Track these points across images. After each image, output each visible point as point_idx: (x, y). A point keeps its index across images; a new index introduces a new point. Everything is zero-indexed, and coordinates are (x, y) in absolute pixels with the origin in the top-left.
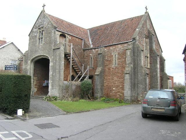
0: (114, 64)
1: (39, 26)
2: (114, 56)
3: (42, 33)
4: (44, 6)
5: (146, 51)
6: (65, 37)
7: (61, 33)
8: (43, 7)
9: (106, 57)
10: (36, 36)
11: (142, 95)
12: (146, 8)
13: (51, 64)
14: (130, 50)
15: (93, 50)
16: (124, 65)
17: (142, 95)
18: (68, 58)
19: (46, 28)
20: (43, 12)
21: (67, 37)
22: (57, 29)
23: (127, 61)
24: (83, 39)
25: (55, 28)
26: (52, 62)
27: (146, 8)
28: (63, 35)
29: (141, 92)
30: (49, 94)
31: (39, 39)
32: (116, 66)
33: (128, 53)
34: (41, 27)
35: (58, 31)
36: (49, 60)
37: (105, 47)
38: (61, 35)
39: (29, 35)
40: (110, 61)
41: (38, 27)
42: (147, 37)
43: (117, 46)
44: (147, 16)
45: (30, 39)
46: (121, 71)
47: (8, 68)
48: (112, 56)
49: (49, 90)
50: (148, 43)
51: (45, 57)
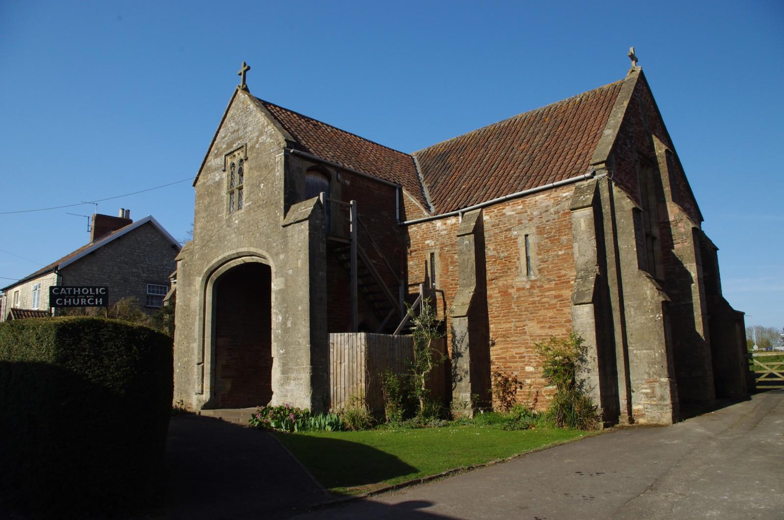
0: (525, 272)
1: (229, 145)
2: (521, 240)
3: (241, 172)
7: (313, 164)
10: (219, 184)
17: (648, 391)
18: (344, 257)
19: (253, 147)
23: (577, 255)
29: (646, 377)
32: (533, 278)
34: (235, 146)
36: (267, 269)
41: (227, 149)
43: (530, 200)
46: (556, 297)
47: (63, 296)
48: (514, 240)
49: (275, 386)
51: (255, 259)
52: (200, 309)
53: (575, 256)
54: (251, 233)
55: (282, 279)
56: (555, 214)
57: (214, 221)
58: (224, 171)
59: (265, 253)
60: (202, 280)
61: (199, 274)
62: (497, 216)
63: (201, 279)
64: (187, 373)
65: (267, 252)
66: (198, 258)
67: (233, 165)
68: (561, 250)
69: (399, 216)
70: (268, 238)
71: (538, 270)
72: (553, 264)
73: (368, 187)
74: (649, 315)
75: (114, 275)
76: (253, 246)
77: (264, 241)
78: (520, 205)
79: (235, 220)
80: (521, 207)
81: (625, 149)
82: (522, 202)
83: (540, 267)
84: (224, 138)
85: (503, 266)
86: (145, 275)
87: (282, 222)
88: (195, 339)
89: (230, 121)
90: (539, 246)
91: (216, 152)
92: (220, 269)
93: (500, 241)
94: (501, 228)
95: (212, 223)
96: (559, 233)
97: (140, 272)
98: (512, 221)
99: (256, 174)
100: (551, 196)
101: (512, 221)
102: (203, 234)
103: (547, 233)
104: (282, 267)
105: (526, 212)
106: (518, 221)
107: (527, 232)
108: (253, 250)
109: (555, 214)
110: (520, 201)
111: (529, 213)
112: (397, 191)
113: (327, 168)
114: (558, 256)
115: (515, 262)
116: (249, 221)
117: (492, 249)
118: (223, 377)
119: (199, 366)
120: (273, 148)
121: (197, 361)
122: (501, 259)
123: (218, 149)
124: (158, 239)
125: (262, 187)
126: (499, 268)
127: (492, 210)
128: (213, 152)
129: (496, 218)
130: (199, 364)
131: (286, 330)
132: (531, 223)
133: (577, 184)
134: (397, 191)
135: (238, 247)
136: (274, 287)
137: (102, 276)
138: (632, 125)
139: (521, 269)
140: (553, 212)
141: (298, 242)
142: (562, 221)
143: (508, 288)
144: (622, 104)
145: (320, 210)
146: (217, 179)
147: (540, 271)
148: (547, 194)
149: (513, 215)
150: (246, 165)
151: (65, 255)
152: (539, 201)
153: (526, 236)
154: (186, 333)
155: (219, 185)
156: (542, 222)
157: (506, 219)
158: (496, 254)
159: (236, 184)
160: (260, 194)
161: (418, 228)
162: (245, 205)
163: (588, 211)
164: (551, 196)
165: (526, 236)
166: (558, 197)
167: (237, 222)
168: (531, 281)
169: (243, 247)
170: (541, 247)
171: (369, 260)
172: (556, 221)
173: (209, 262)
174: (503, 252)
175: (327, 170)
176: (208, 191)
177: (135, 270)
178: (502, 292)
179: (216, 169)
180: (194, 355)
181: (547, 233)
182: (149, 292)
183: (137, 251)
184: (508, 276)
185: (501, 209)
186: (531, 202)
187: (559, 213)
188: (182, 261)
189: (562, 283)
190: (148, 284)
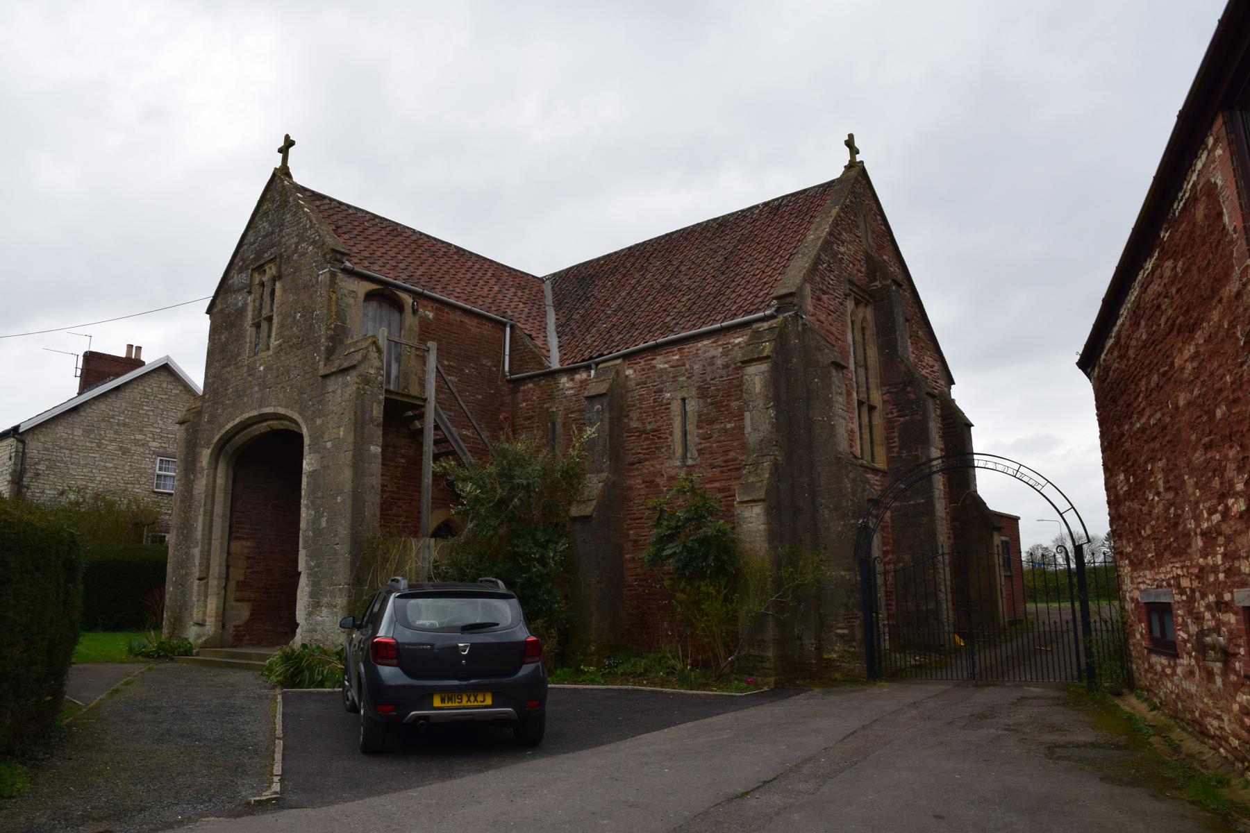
2: (676, 407)
4: (289, 143)
5: (861, 372)
6: (399, 306)
8: (280, 151)
9: (635, 415)
11: (846, 631)
12: (850, 143)
13: (308, 464)
14: (764, 367)
15: (564, 379)
16: (732, 455)
20: (282, 173)
21: (408, 309)
22: (348, 264)
23: (748, 429)
24: (504, 325)
25: (337, 256)
26: (316, 447)
27: (850, 143)
28: (385, 296)
30: (299, 639)
31: (257, 326)
32: (690, 462)
33: (756, 376)
35: (350, 273)
37: (625, 357)
38: (369, 296)
39: (208, 312)
40: (656, 439)
41: (255, 260)
42: (864, 296)
44: (857, 181)
45: (214, 331)
46: (720, 490)
50: (868, 332)
52: (206, 496)
53: (746, 432)
54: (280, 386)
55: (318, 456)
56: (723, 369)
57: (232, 367)
58: (250, 293)
59: (296, 416)
60: (212, 454)
61: (207, 445)
62: (643, 370)
63: (209, 451)
64: (184, 594)
65: (300, 414)
66: (208, 421)
67: (262, 284)
68: (729, 422)
69: (510, 368)
70: (302, 393)
71: (698, 450)
72: (718, 442)
73: (461, 322)
74: (848, 520)
75: (108, 443)
76: (280, 405)
77: (296, 397)
78: (676, 355)
79: (261, 365)
80: (677, 357)
81: (829, 277)
82: (679, 350)
83: (700, 447)
84: (252, 244)
85: (650, 444)
86: (155, 444)
87: (323, 371)
88: (197, 542)
89: (261, 220)
90: (700, 415)
91: (241, 264)
92: (237, 437)
93: (648, 408)
94: (648, 387)
95: (229, 369)
96: (728, 396)
97: (148, 439)
98: (665, 377)
99: (292, 298)
100: (720, 343)
101: (665, 377)
102: (215, 385)
103: (712, 396)
104: (317, 437)
105: (684, 365)
106: (673, 377)
107: (684, 394)
108: (281, 410)
109: (723, 369)
110: (676, 349)
111: (687, 366)
112: (508, 330)
113: (397, 293)
114: (726, 430)
115: (667, 438)
116: (278, 369)
117: (635, 418)
118: (237, 600)
119: (202, 582)
120: (315, 262)
121: (197, 574)
122: (648, 433)
123: (243, 260)
124: (178, 392)
125: (298, 318)
126: (645, 447)
127: (638, 360)
128: (237, 264)
129: (642, 373)
130: (200, 579)
131: (318, 532)
132: (690, 381)
133: (755, 326)
134: (508, 330)
135: (261, 406)
136: (306, 466)
137: (88, 444)
138: (843, 243)
139: (674, 449)
140: (721, 366)
141: (342, 401)
142: (733, 379)
143: (656, 476)
144: (830, 212)
145: (377, 354)
146: (240, 304)
147: (700, 452)
148: (713, 340)
149: (666, 369)
150: (278, 285)
151: (1097, 423)
152: (703, 350)
153: (684, 400)
154: (185, 532)
155: (241, 313)
156: (706, 380)
157: (657, 374)
158: (640, 426)
159: (265, 313)
160: (295, 329)
161: (535, 385)
162: (274, 343)
163: (765, 365)
164: (720, 343)
165: (684, 400)
166: (728, 343)
167: (262, 368)
168: (688, 466)
169: (267, 406)
170: (703, 417)
171: (453, 430)
172: (725, 378)
173: (221, 426)
174: (650, 423)
175: (398, 296)
176: (226, 322)
177: (140, 437)
178: (647, 482)
179: (239, 290)
180: (195, 566)
181: (712, 396)
182: (160, 469)
183: (145, 408)
184: (655, 458)
185: (649, 360)
186: (691, 350)
187: (728, 367)
188: (186, 424)
189: (730, 470)
190: (159, 458)
